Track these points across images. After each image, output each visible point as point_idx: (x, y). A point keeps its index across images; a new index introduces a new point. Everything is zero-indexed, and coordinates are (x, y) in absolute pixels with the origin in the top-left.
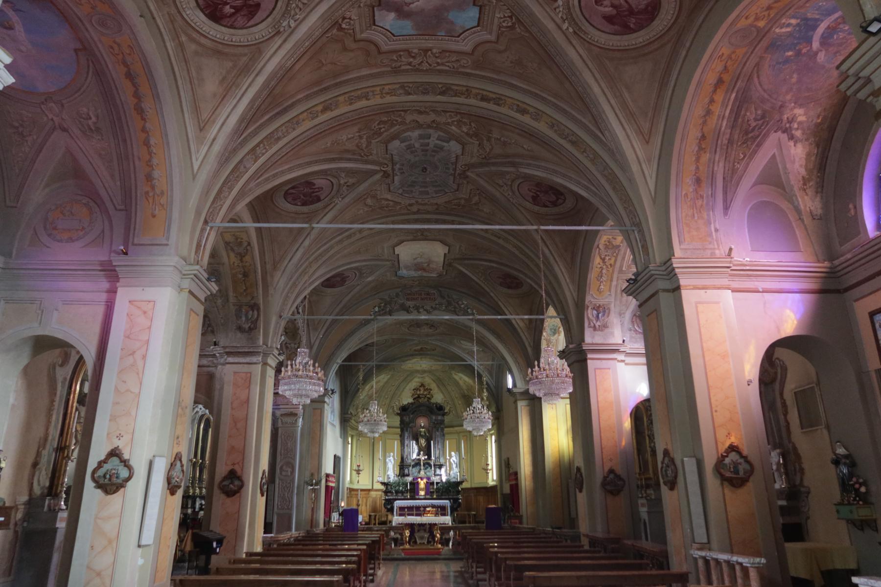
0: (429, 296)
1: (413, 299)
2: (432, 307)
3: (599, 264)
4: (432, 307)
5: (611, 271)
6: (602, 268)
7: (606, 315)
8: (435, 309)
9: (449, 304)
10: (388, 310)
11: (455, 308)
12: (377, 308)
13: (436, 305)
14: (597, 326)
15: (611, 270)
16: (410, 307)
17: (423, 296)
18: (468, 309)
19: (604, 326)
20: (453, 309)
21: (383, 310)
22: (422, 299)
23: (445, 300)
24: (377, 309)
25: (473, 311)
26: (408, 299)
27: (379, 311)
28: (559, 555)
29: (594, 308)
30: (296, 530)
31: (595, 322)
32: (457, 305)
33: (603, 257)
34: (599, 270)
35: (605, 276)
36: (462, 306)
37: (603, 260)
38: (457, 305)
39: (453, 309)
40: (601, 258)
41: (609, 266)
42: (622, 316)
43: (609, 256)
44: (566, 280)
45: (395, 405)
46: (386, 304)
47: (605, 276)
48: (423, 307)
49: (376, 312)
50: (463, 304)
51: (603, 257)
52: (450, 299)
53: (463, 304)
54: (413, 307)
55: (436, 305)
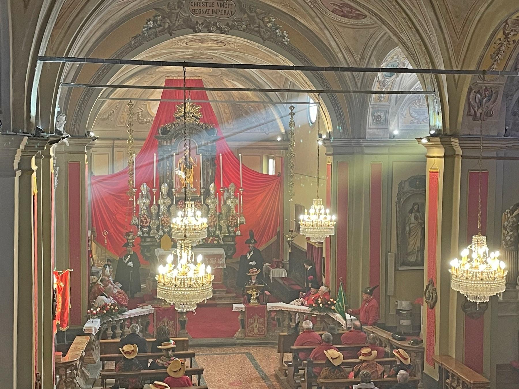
0: (224, 9)
1: (201, 12)
2: (228, 25)
3: (500, 39)
4: (228, 25)
5: (512, 49)
6: (501, 44)
7: (492, 100)
8: (232, 27)
9: (252, 20)
10: (167, 25)
11: (259, 26)
12: (151, 22)
13: (234, 21)
14: (478, 114)
15: (512, 47)
16: (197, 22)
17: (216, 8)
18: (276, 29)
19: (487, 115)
20: (256, 29)
21: (160, 26)
22: (214, 12)
23: (246, 15)
24: (151, 24)
25: (283, 33)
26: (194, 12)
27: (154, 27)
28: (234, 167)
29: (479, 91)
30: (67, 340)
31: (476, 109)
32: (262, 23)
33: (507, 32)
34: (497, 47)
35: (502, 53)
36: (269, 25)
37: (506, 36)
38: (262, 23)
39: (256, 29)
40: (504, 33)
41: (511, 43)
42: (509, 98)
43: (515, 30)
44: (448, 52)
45: (140, 111)
46: (163, 18)
47: (502, 53)
48: (215, 24)
49: (150, 28)
50: (270, 22)
51: (507, 32)
52: (252, 14)
53: (270, 22)
54: (202, 24)
55: (234, 21)
